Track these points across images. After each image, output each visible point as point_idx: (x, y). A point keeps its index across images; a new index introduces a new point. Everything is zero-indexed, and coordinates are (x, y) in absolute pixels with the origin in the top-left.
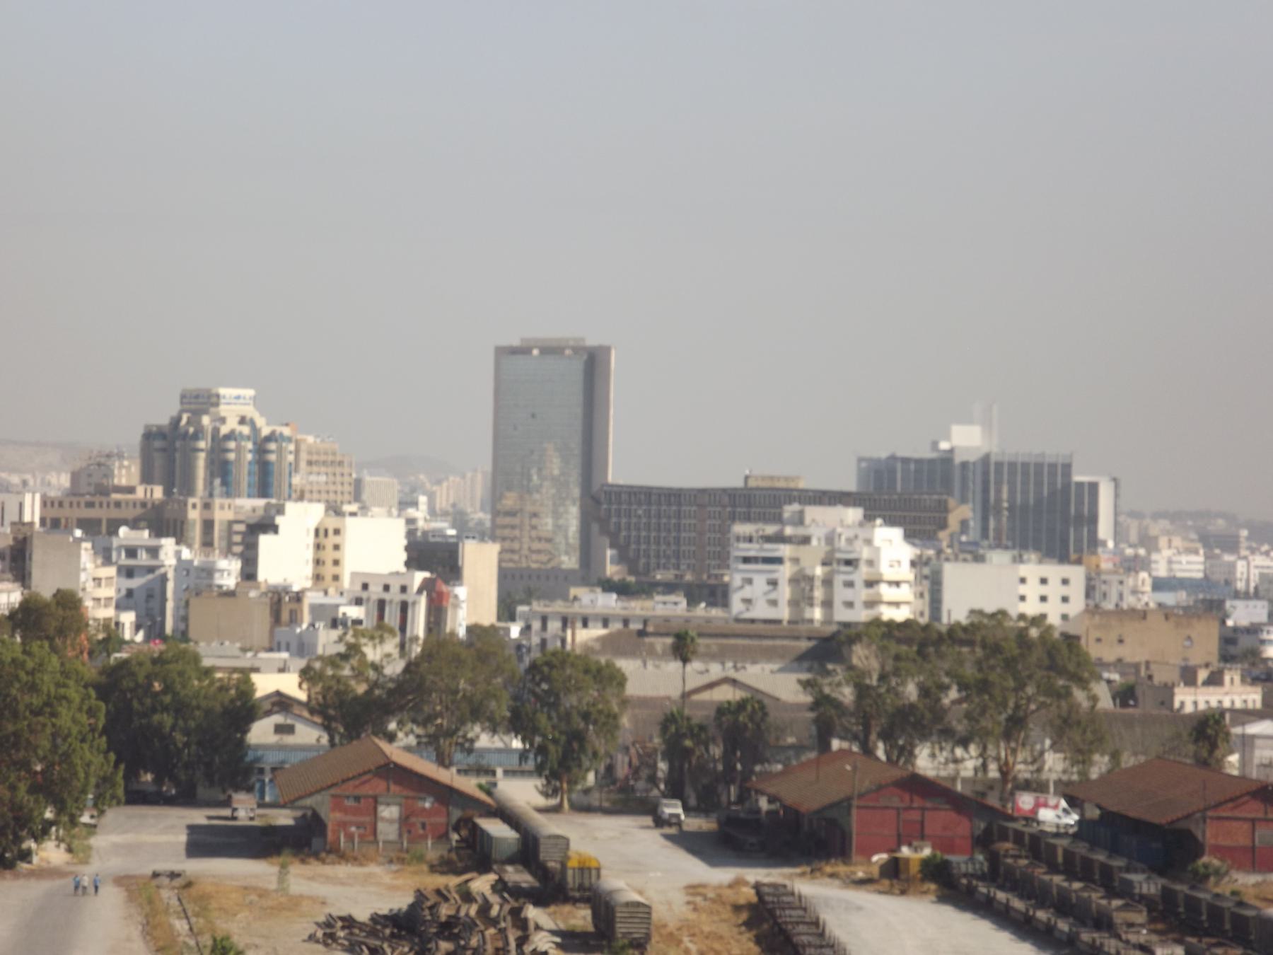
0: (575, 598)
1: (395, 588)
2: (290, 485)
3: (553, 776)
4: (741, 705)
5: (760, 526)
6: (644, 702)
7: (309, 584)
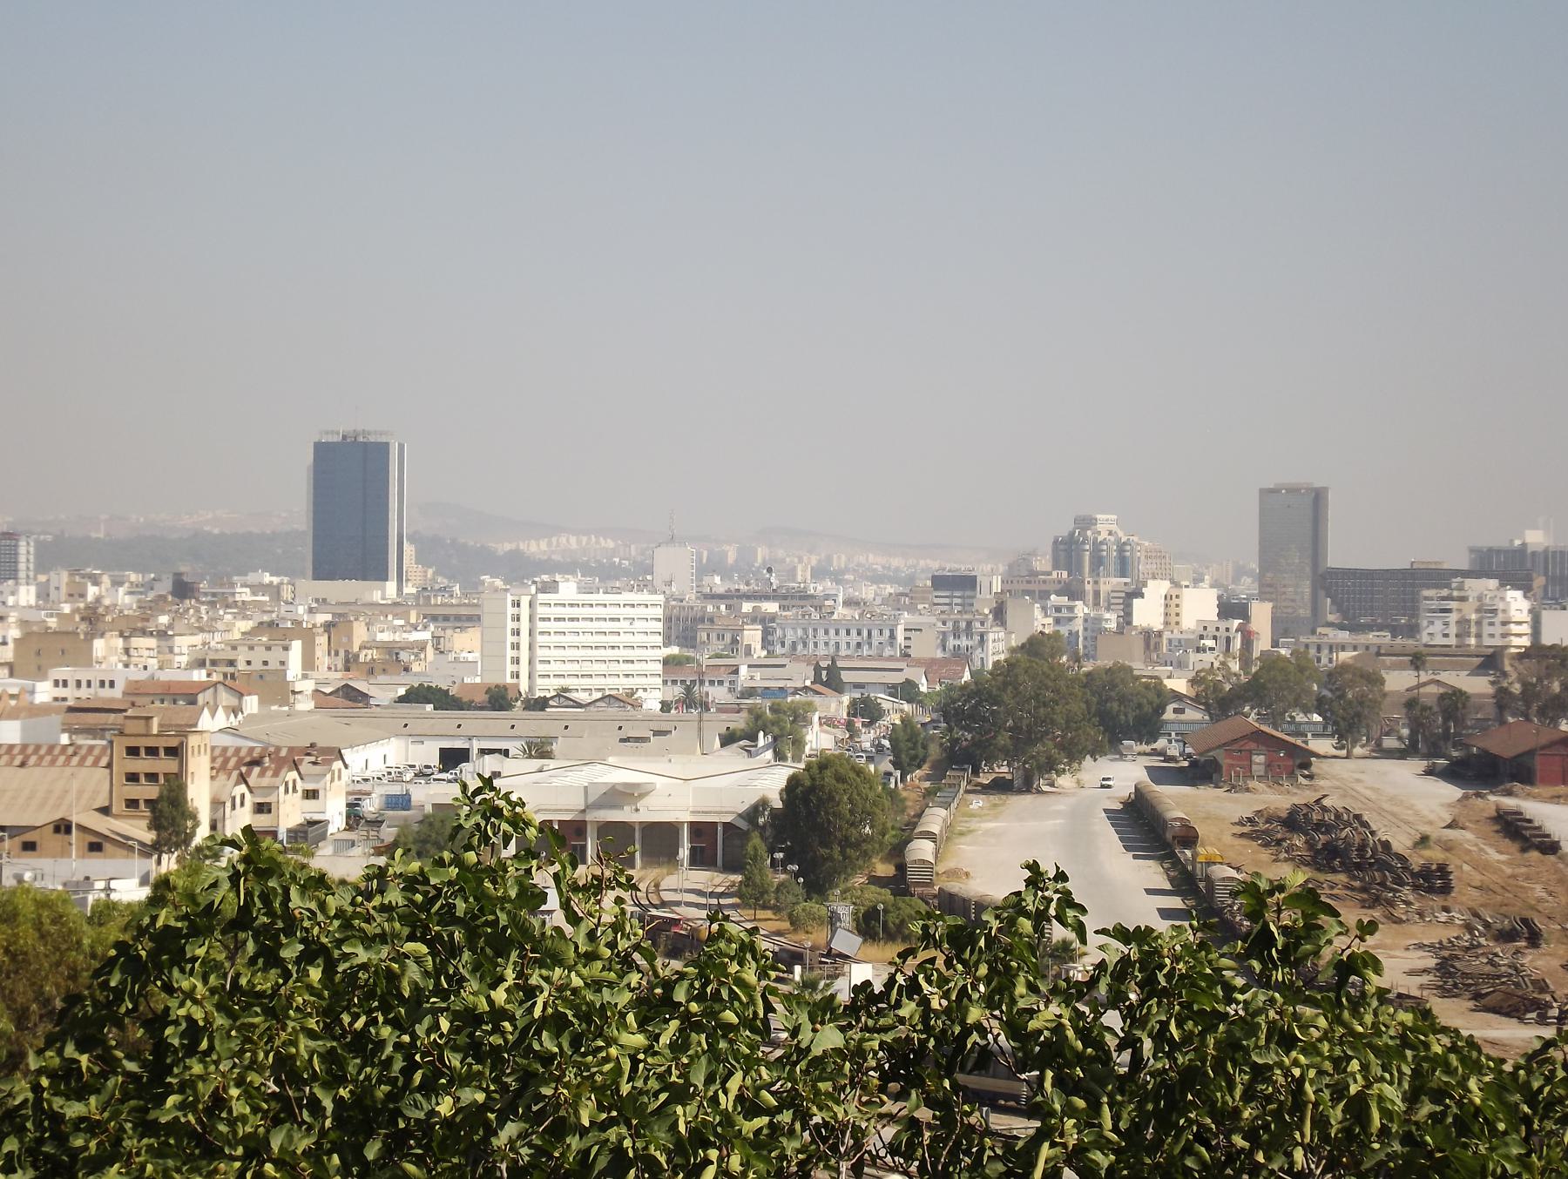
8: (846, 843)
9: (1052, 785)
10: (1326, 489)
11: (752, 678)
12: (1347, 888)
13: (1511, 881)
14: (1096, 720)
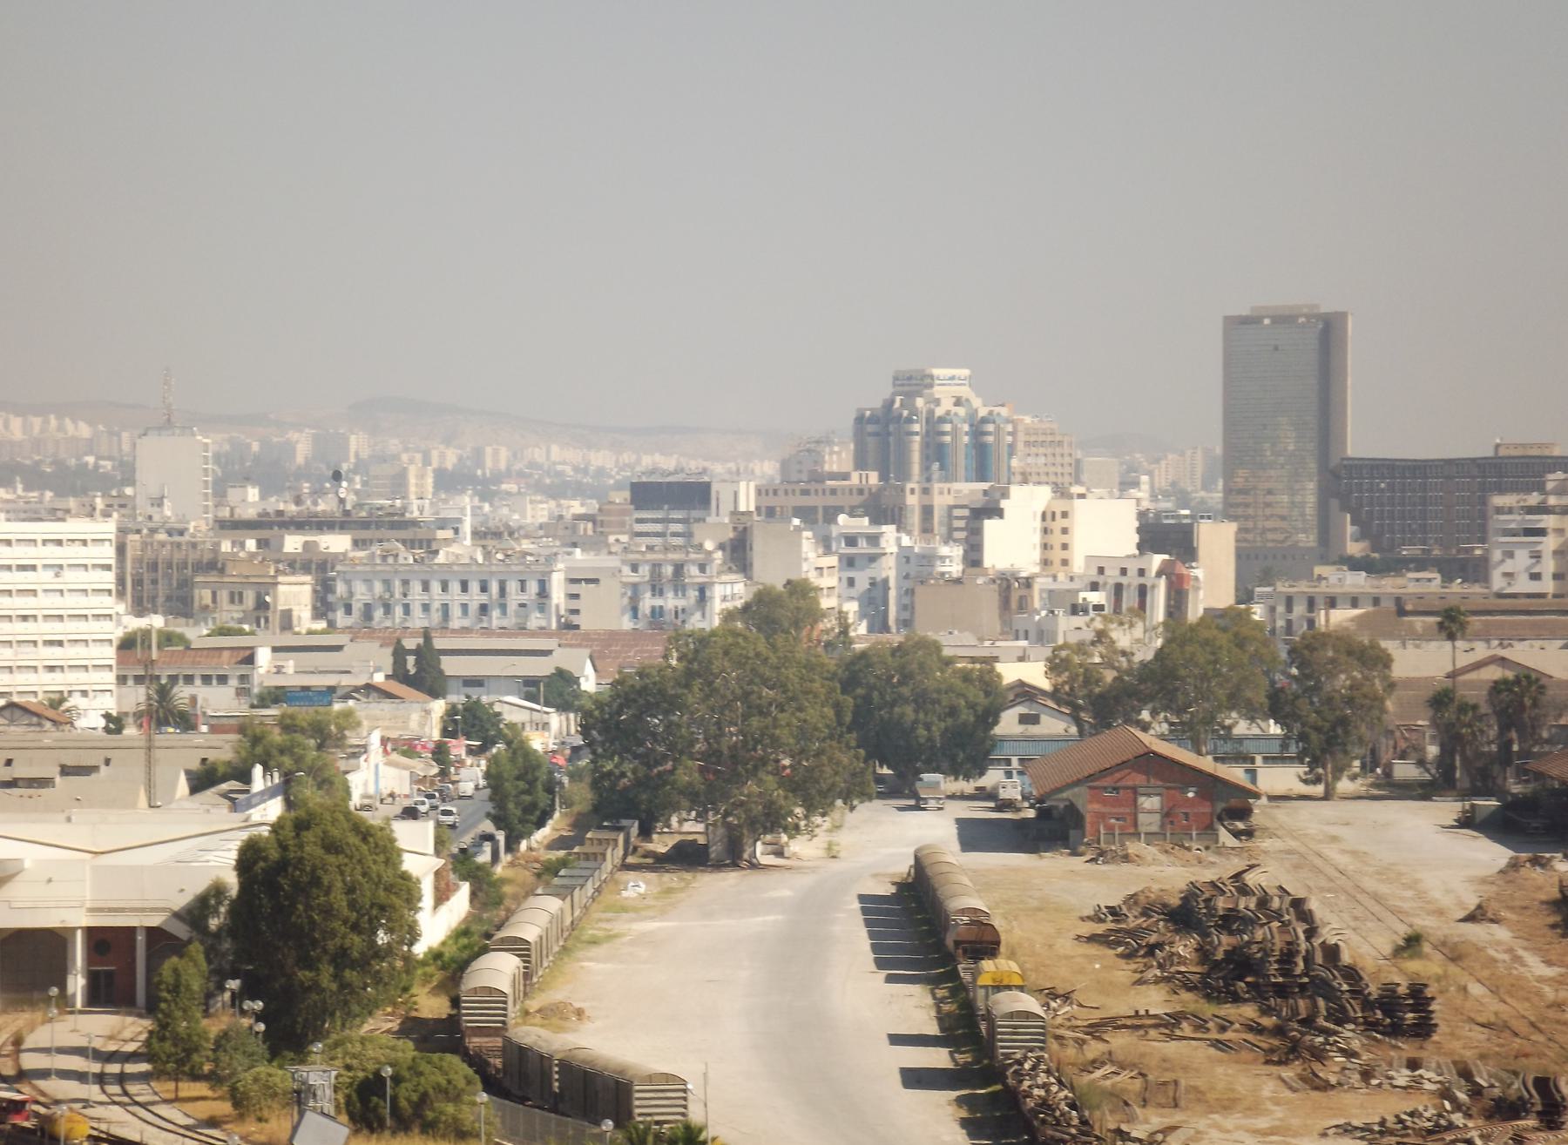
0: (1320, 578)
1: (1133, 572)
2: (1009, 467)
3: (1316, 762)
4: (1517, 681)
5: (1522, 496)
6: (1409, 683)
7: (1037, 569)
8: (341, 959)
9: (779, 853)
10: (1342, 316)
11: (279, 670)
12: (1250, 1029)
13: (1551, 1014)
14: (852, 738)
